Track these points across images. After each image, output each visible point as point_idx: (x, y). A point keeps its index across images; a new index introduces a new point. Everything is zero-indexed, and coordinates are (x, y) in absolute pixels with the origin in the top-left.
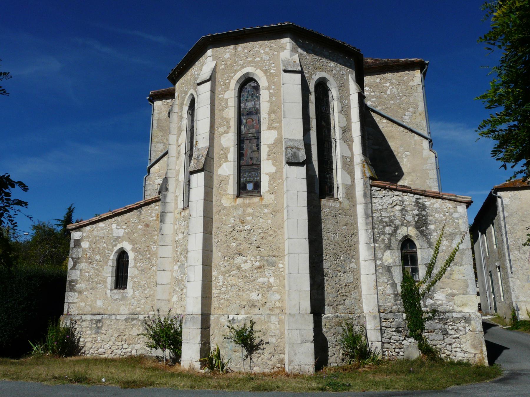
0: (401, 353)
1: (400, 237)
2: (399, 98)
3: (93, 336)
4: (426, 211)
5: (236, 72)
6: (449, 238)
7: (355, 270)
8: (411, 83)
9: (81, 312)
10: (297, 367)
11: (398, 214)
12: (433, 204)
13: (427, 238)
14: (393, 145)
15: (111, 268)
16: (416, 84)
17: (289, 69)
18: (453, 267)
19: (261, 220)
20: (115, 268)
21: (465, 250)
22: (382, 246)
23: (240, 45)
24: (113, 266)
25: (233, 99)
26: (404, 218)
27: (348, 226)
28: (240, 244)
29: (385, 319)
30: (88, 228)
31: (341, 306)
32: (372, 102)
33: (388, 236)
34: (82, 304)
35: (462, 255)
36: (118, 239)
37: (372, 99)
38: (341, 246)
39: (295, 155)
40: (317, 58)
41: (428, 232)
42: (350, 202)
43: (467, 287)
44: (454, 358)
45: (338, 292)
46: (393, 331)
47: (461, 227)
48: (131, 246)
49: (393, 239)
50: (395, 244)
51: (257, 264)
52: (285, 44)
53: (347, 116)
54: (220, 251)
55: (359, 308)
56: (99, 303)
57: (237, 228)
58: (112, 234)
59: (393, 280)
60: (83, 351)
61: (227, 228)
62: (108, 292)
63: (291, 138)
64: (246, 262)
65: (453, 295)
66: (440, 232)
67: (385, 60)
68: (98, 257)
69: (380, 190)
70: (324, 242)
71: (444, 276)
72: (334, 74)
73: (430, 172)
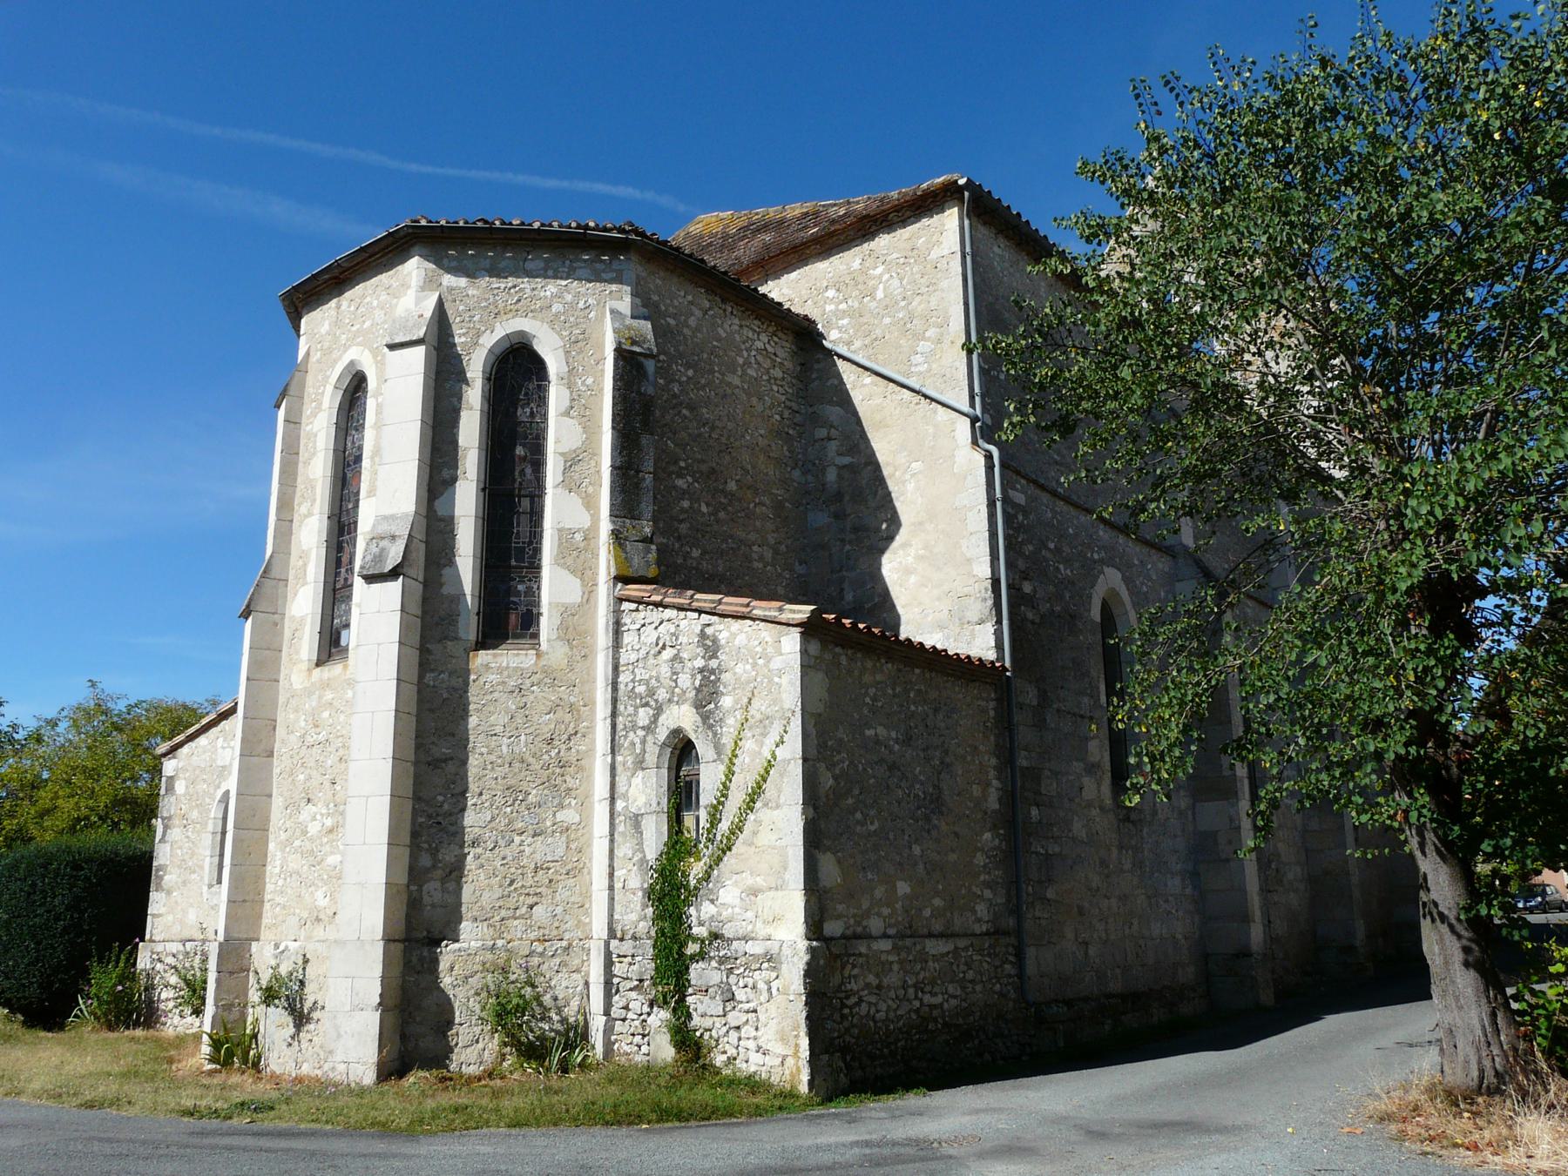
0: (644, 1049)
1: (662, 734)
2: (903, 303)
4: (717, 658)
5: (335, 362)
7: (574, 827)
8: (935, 254)
10: (342, 1067)
11: (665, 671)
12: (734, 635)
13: (715, 734)
14: (883, 446)
15: (210, 836)
17: (398, 340)
18: (762, 814)
21: (789, 761)
22: (630, 759)
26: (676, 681)
27: (560, 714)
28: (310, 778)
29: (619, 956)
30: (185, 750)
31: (516, 922)
32: (840, 332)
33: (641, 733)
35: (781, 775)
37: (841, 322)
38: (530, 768)
39: (380, 557)
40: (503, 286)
41: (718, 715)
42: (571, 649)
44: (744, 1065)
45: (510, 885)
46: (631, 990)
47: (784, 696)
51: (329, 822)
52: (410, 274)
53: (584, 419)
55: (577, 926)
57: (310, 740)
58: (215, 760)
59: (643, 852)
62: (205, 888)
64: (314, 819)
65: (754, 892)
67: (894, 194)
69: (637, 610)
70: (474, 762)
71: (741, 836)
72: (557, 315)
73: (970, 514)
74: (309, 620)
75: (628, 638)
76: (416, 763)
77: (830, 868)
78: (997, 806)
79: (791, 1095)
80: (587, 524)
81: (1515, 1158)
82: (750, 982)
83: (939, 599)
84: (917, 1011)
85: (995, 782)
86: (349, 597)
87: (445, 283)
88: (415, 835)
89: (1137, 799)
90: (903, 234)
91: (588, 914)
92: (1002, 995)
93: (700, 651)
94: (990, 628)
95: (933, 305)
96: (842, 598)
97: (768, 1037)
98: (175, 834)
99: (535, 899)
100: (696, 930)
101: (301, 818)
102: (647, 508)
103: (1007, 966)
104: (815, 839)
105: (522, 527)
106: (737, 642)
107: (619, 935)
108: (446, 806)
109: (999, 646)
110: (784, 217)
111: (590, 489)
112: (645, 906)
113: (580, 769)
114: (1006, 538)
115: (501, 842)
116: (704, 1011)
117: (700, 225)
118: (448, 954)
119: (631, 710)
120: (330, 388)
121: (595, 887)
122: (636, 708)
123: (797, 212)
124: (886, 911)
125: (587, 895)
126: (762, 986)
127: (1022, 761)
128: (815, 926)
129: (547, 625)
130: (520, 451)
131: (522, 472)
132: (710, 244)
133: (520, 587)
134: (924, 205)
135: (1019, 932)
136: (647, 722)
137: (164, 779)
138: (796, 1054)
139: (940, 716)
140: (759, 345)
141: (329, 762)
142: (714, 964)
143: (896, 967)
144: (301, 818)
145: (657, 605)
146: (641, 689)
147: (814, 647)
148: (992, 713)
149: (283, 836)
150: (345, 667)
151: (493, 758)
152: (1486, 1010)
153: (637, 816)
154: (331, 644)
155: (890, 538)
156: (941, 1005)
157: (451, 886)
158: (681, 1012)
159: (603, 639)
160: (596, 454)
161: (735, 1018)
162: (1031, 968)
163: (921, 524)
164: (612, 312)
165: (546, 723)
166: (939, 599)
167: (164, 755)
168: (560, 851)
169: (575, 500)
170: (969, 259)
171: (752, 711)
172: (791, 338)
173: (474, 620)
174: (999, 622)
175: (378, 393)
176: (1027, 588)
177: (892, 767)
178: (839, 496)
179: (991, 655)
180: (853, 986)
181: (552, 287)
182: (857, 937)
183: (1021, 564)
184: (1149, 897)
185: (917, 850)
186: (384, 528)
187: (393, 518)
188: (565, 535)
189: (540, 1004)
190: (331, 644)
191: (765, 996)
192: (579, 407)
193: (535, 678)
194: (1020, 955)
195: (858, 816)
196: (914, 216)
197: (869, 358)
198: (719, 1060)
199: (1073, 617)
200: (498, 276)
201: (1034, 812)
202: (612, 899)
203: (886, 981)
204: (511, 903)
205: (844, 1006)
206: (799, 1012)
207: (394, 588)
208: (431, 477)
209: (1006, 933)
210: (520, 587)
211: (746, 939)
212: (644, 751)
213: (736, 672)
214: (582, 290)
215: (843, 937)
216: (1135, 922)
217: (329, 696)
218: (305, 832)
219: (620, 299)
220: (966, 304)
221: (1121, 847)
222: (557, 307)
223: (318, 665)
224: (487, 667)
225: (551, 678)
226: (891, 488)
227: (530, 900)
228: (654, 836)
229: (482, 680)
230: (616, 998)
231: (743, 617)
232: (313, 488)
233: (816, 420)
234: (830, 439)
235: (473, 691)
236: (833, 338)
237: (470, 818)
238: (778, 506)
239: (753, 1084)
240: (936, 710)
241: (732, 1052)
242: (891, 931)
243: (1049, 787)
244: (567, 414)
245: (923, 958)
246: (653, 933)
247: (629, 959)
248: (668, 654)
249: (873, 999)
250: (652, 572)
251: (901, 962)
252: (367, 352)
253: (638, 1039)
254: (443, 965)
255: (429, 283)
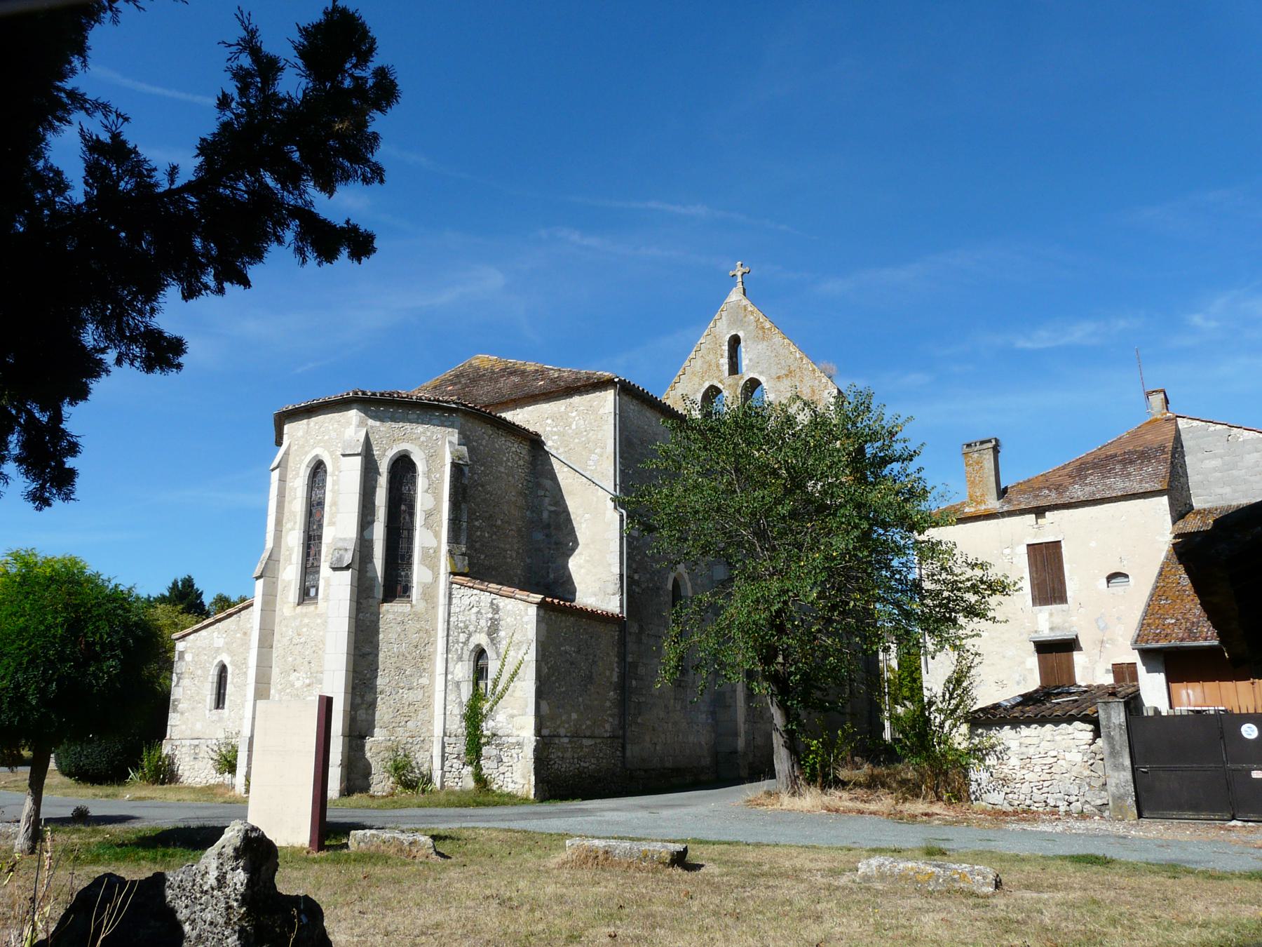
0: (460, 784)
1: (471, 646)
2: (585, 433)
3: (192, 763)
5: (306, 453)
6: (516, 648)
8: (601, 411)
9: (182, 737)
11: (473, 618)
12: (507, 605)
13: (496, 648)
16: (607, 412)
18: (517, 683)
19: (314, 632)
20: (215, 685)
22: (455, 657)
23: (313, 419)
24: (212, 683)
25: (301, 488)
27: (421, 633)
28: (295, 659)
30: (192, 637)
33: (461, 645)
34: (184, 727)
35: (526, 667)
36: (218, 650)
37: (553, 438)
39: (340, 559)
41: (498, 639)
43: (527, 706)
47: (529, 633)
48: (230, 659)
49: (465, 648)
50: (466, 655)
51: (307, 681)
54: (278, 667)
56: (198, 726)
57: (295, 641)
58: (212, 644)
60: (181, 780)
61: (285, 641)
62: (207, 712)
63: (342, 537)
64: (298, 679)
65: (512, 716)
66: (508, 640)
68: (199, 672)
70: (381, 655)
72: (423, 442)
74: (293, 582)
75: (454, 601)
76: (354, 655)
77: (545, 706)
78: (616, 680)
79: (527, 799)
80: (435, 545)
81: (777, 806)
82: (510, 754)
83: (595, 581)
84: (578, 769)
85: (616, 669)
86: (318, 572)
87: (369, 424)
88: (353, 688)
89: (659, 685)
90: (585, 397)
91: (432, 725)
92: (614, 764)
93: (490, 610)
94: (617, 597)
95: (599, 437)
96: (548, 576)
97: (517, 777)
98: (185, 682)
99: (409, 718)
100: (485, 733)
101: (291, 679)
102: (463, 538)
103: (618, 752)
104: (541, 693)
105: (403, 545)
106: (508, 608)
107: (448, 734)
108: (368, 675)
109: (621, 606)
110: (525, 369)
111: (437, 528)
112: (461, 722)
113: (430, 660)
114: (627, 554)
115: (393, 692)
116: (488, 767)
117: (477, 361)
118: (369, 742)
119: (456, 634)
120: (304, 466)
121: (436, 713)
122: (459, 633)
123: (532, 368)
124: (567, 726)
125: (432, 717)
126: (515, 755)
127: (629, 659)
128: (538, 731)
129: (415, 592)
130: (403, 507)
131: (404, 518)
132: (484, 375)
133: (402, 573)
134: (599, 385)
135: (624, 737)
136: (464, 640)
137: (177, 653)
138: (529, 783)
139: (593, 640)
140: (514, 449)
141: (307, 653)
142: (494, 747)
143: (570, 750)
144: (291, 679)
145: (470, 587)
146: (461, 625)
147: (542, 613)
148: (617, 637)
149: (279, 687)
150: (316, 608)
151: (390, 654)
152: (790, 763)
153: (458, 682)
154: (306, 594)
155: (573, 550)
156: (588, 767)
157: (370, 712)
158: (478, 768)
159: (442, 599)
160: (440, 511)
161: (502, 769)
162: (628, 753)
163: (588, 544)
164: (450, 442)
165: (414, 638)
166: (595, 581)
167: (177, 639)
168: (420, 697)
169: (430, 534)
170: (617, 416)
171: (514, 638)
172: (528, 443)
173: (382, 589)
174: (622, 595)
175: (333, 475)
176: (636, 577)
177: (572, 663)
178: (548, 526)
179: (617, 610)
180: (552, 756)
181: (420, 429)
182: (554, 736)
183: (634, 566)
184: (688, 724)
185: (580, 699)
186: (340, 545)
187: (345, 539)
188: (425, 550)
189: (411, 766)
190: (306, 594)
191: (516, 760)
192: (433, 488)
193: (410, 617)
194: (624, 747)
195: (557, 684)
196: (592, 389)
197: (567, 459)
198: (495, 787)
199: (658, 588)
200: (395, 422)
201: (634, 682)
202: (445, 719)
203: (565, 756)
204: (398, 720)
205: (548, 764)
206: (531, 765)
207: (347, 575)
208: (362, 520)
209: (618, 738)
210: (402, 573)
211: (508, 736)
212: (462, 653)
213: (507, 621)
214: (435, 430)
215: (549, 736)
216: (680, 735)
217: (306, 621)
218: (293, 686)
219: (453, 435)
220: (615, 439)
221: (675, 699)
222: (423, 439)
223: (298, 605)
224: (388, 611)
225: (417, 617)
226: (575, 525)
227: (406, 719)
228: (466, 692)
229: (385, 618)
230: (447, 762)
231: (511, 598)
232: (295, 516)
233: (539, 485)
234: (546, 497)
235: (381, 622)
236: (550, 445)
237: (379, 681)
238: (519, 530)
239: (511, 796)
240: (591, 637)
241: (500, 783)
242: (569, 735)
243: (641, 670)
244: (427, 491)
245: (581, 746)
246: (465, 734)
247: (453, 745)
248: (475, 610)
249: (560, 763)
250: (466, 570)
251: (572, 747)
252: (326, 452)
253: (457, 780)
254: (367, 747)
255: (361, 424)
